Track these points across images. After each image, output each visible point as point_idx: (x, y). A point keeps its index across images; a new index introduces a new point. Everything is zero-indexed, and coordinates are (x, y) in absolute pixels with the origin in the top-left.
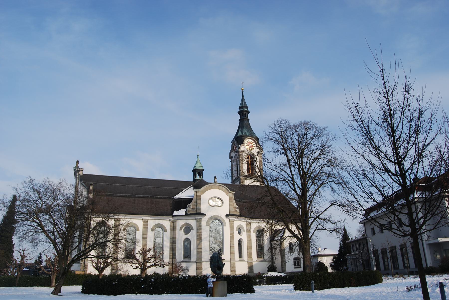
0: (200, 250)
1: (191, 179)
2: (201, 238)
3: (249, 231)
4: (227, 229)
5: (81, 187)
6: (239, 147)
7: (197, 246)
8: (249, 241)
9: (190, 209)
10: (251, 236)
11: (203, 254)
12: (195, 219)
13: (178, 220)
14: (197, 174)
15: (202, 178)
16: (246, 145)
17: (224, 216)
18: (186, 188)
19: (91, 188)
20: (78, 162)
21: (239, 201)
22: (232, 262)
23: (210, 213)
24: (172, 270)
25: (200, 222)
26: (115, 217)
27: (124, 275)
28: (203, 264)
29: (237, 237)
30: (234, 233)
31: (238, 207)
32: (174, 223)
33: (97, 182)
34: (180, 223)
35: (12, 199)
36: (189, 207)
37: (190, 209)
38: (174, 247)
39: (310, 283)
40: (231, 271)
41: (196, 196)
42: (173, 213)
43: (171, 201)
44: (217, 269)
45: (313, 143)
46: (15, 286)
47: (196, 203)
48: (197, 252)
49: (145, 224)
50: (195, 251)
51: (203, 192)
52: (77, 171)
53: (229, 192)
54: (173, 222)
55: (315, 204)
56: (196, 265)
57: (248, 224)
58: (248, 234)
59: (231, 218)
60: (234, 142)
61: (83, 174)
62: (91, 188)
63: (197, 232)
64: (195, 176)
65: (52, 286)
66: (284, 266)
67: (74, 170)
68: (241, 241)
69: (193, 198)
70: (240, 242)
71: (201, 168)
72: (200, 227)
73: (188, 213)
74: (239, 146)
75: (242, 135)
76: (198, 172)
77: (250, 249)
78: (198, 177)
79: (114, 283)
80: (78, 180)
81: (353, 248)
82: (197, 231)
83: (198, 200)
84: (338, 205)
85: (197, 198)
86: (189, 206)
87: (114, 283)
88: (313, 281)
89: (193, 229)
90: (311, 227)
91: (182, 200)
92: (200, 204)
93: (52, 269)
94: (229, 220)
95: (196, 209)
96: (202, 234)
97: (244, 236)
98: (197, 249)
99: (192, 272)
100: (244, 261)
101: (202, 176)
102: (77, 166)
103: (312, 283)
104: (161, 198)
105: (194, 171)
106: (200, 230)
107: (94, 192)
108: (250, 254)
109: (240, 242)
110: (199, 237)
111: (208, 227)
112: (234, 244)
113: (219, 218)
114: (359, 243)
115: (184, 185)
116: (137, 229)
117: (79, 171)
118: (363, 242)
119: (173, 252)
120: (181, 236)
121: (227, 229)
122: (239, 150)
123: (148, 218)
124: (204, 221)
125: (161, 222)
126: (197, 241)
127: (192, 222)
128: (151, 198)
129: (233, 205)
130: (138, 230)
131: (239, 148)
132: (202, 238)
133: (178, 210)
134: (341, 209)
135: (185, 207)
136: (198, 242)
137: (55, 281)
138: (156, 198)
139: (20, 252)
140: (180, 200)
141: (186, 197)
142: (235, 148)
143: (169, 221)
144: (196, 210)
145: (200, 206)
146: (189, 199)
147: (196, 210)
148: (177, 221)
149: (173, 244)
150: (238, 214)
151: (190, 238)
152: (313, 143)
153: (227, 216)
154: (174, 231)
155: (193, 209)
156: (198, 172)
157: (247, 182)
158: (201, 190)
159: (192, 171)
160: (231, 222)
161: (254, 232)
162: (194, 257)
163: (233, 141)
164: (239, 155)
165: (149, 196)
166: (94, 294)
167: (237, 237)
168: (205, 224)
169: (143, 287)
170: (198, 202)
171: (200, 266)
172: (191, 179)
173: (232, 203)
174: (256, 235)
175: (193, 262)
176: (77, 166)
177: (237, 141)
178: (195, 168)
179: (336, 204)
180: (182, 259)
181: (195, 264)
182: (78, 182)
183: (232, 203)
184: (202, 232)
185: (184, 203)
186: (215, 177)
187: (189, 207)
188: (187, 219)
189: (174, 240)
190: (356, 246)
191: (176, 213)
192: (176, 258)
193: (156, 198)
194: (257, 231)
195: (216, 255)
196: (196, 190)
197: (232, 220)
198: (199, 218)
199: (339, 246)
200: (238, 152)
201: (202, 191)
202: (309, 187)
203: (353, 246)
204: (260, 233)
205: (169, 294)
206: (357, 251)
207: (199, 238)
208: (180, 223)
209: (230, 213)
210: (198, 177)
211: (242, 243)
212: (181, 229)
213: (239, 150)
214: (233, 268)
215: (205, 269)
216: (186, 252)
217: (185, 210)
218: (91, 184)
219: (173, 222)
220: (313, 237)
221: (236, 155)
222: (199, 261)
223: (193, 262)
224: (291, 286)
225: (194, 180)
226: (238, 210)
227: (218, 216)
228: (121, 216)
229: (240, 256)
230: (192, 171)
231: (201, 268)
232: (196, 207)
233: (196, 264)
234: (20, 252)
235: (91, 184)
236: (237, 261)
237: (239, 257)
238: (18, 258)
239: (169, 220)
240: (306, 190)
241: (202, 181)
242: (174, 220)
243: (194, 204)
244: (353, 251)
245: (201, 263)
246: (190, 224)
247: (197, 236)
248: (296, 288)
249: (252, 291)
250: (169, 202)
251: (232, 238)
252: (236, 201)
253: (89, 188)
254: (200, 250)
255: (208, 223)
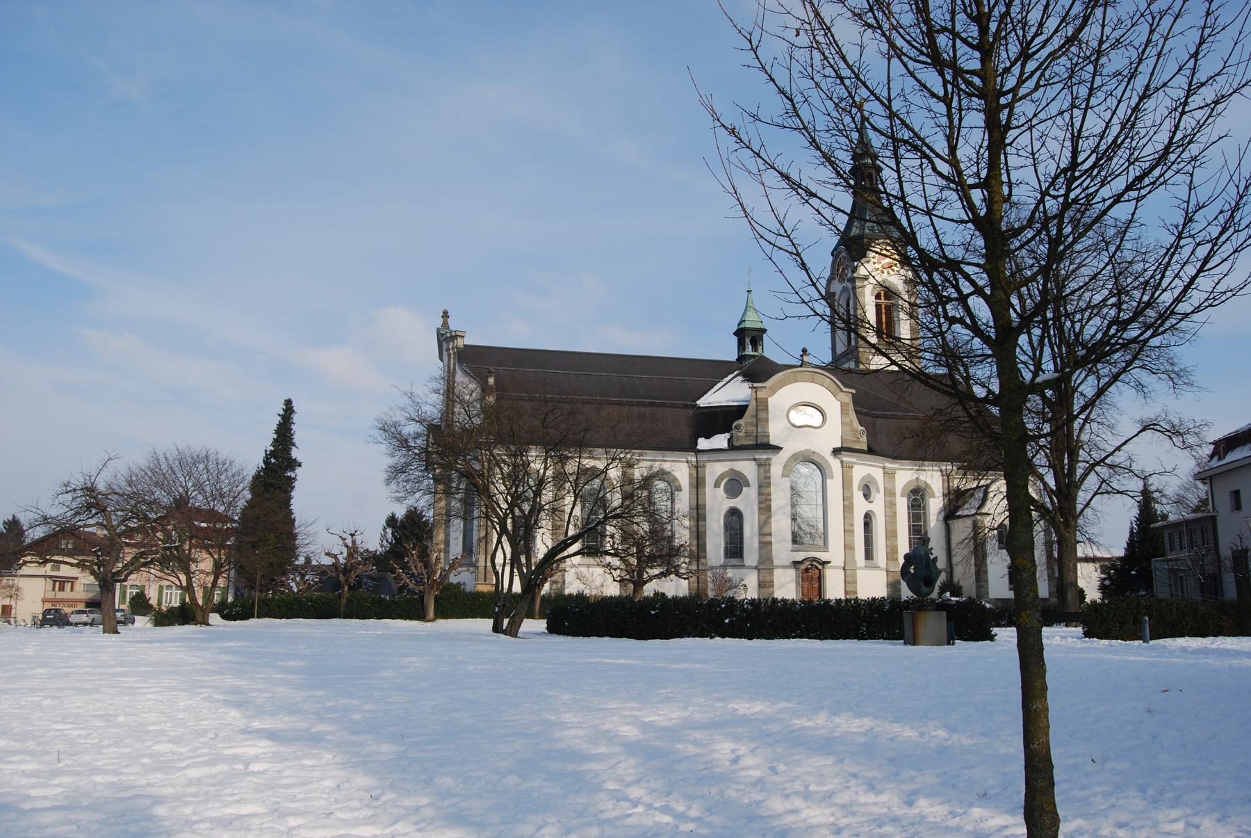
0: (767, 539)
1: (731, 354)
2: (769, 508)
3: (890, 493)
4: (835, 486)
5: (460, 377)
6: (856, 268)
7: (760, 528)
8: (891, 516)
9: (741, 434)
10: (895, 505)
11: (775, 548)
12: (755, 460)
13: (708, 461)
14: (748, 340)
15: (760, 351)
16: (872, 260)
17: (826, 453)
18: (722, 379)
19: (491, 381)
20: (445, 315)
21: (865, 414)
22: (848, 571)
23: (791, 447)
24: (696, 585)
25: (767, 467)
26: (887, 465)
27: (595, 596)
28: (777, 572)
29: (861, 506)
30: (852, 495)
31: (863, 428)
32: (699, 469)
33: (500, 366)
34: (715, 470)
35: (283, 409)
36: (737, 427)
37: (741, 434)
38: (701, 529)
39: (1138, 622)
40: (846, 593)
41: (756, 399)
42: (697, 445)
43: (691, 412)
44: (922, 583)
45: (1090, 264)
46: (340, 618)
47: (754, 420)
48: (760, 543)
49: (889, 475)
50: (756, 540)
51: (774, 391)
52: (445, 338)
53: (842, 391)
54: (697, 467)
55: (1100, 426)
56: (759, 576)
57: (889, 475)
58: (888, 498)
59: (845, 459)
60: (840, 253)
61: (465, 346)
62: (491, 381)
63: (760, 494)
64: (741, 345)
65: (428, 618)
66: (983, 584)
67: (438, 333)
68: (870, 517)
69: (747, 406)
70: (734, 516)
71: (758, 326)
72: (766, 481)
73: (736, 444)
74: (856, 263)
75: (863, 235)
76: (749, 336)
77: (892, 537)
78: (749, 351)
79: (653, 613)
80: (452, 361)
81: (1170, 540)
82: (759, 490)
83: (762, 410)
84: (1159, 431)
85: (757, 406)
86: (738, 427)
87: (653, 613)
88: (1147, 619)
89: (747, 484)
90: (1086, 484)
91: (719, 409)
92: (767, 420)
93: (426, 580)
94: (842, 462)
95: (755, 434)
96: (773, 497)
97: (878, 505)
98: (761, 534)
99: (750, 592)
100: (877, 567)
101: (760, 347)
102: (445, 325)
103: (1146, 621)
104: (662, 405)
105: (741, 333)
106: (766, 487)
107: (497, 390)
108: (892, 549)
109: (734, 516)
110: (763, 506)
111: (788, 479)
112: (852, 525)
113: (815, 458)
114: (1191, 530)
115: (715, 371)
116: (674, 487)
117: (454, 338)
118: (1202, 527)
119: (698, 542)
120: (717, 503)
121: (835, 486)
122: (855, 275)
123: (897, 466)
124: (778, 463)
125: (666, 466)
126: (759, 514)
127: (747, 468)
128: (639, 404)
129: (850, 424)
130: (679, 489)
131: (855, 270)
132: (773, 509)
133: (708, 437)
134: (1168, 441)
135: (726, 429)
136: (763, 517)
137: (433, 607)
138: (652, 404)
139: (344, 539)
140: (713, 410)
141: (728, 401)
142: (843, 270)
143: (686, 464)
144: (757, 437)
145: (767, 426)
146: (735, 408)
147: (757, 437)
148: (708, 464)
149: (698, 521)
150: (865, 448)
151: (741, 507)
152: (1090, 264)
153: (836, 452)
154: (699, 490)
155: (748, 434)
156: (749, 336)
157: (878, 362)
158: (768, 384)
159: (735, 334)
160: (846, 468)
161: (902, 495)
162: (751, 556)
163: (835, 249)
164: (854, 288)
165: (635, 400)
166: (600, 634)
167: (861, 506)
168: (780, 472)
169: (727, 621)
170: (761, 415)
171: (768, 579)
172: (731, 354)
173: (847, 420)
174: (908, 501)
175: (750, 567)
176: (445, 325)
177: (848, 249)
178: (742, 326)
179: (1158, 427)
180: (722, 559)
181: (756, 571)
182: (454, 365)
183: (847, 420)
184: (772, 491)
185: (724, 419)
186: (804, 351)
187: (737, 427)
188: (733, 460)
189: (700, 511)
190: (1180, 538)
191: (703, 443)
192: (705, 557)
193: (652, 404)
194: (911, 491)
195: (923, 553)
196: (755, 385)
197: (848, 462)
198: (764, 457)
199: (1128, 535)
200: (853, 280)
201: (770, 387)
202: (1078, 382)
203: (1170, 537)
204: (917, 496)
205: (794, 638)
206: (1181, 549)
207: (765, 508)
208: (715, 470)
209: (844, 445)
210: (749, 351)
211: (872, 523)
212: (717, 485)
213: (855, 275)
214: (849, 582)
215: (782, 586)
216: (731, 543)
217: (727, 435)
218: (489, 372)
219: (698, 468)
220: (1088, 511)
221: (845, 289)
222: (766, 564)
223: (750, 567)
224: (1079, 630)
225: (741, 358)
226: (864, 439)
227: (814, 452)
228: (634, 455)
229: (869, 555)
230: (735, 334)
231: (771, 584)
232: (755, 428)
233: (759, 572)
234: (344, 539)
235: (489, 372)
236: (861, 568)
237: (866, 559)
238: (342, 553)
239: (687, 462)
240: (1070, 390)
241: (763, 359)
242: (701, 462)
243: (750, 420)
244: (1171, 551)
245: (771, 570)
246: (741, 473)
247: (760, 503)
248: (1088, 634)
249: (991, 638)
250: (685, 415)
251: (848, 508)
252: (857, 412)
253: (487, 382)
254: (767, 539)
255: (787, 471)
